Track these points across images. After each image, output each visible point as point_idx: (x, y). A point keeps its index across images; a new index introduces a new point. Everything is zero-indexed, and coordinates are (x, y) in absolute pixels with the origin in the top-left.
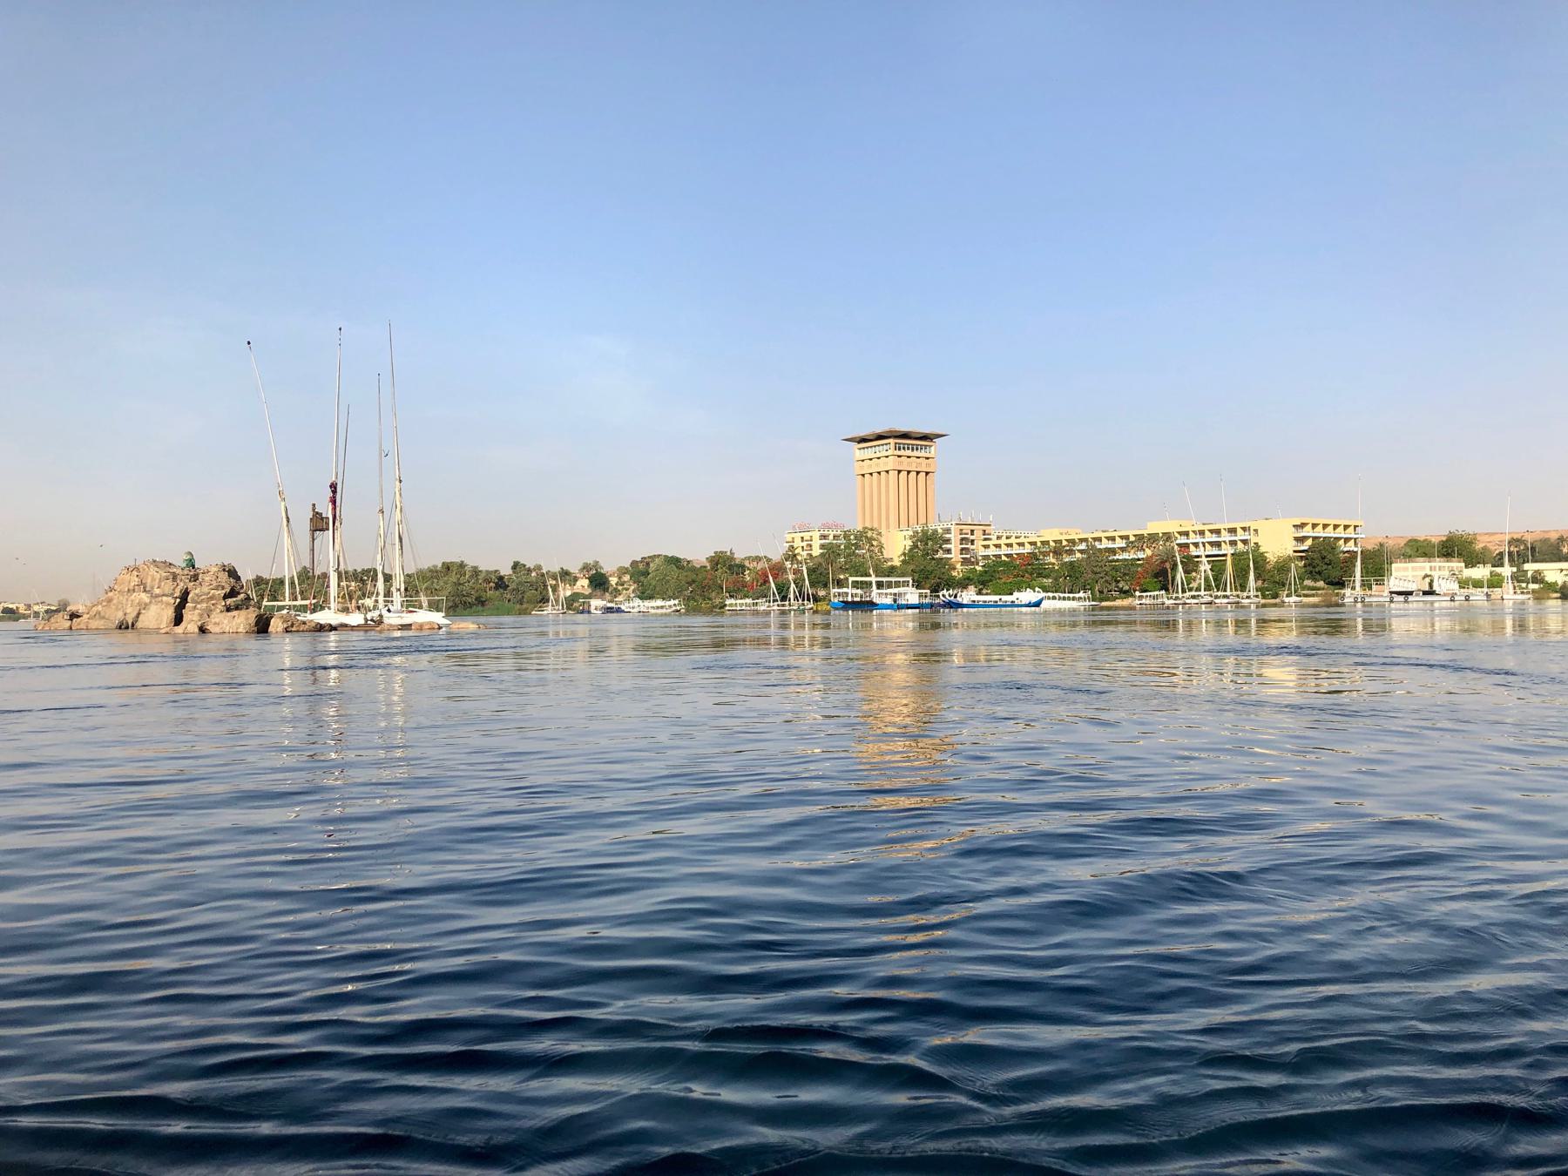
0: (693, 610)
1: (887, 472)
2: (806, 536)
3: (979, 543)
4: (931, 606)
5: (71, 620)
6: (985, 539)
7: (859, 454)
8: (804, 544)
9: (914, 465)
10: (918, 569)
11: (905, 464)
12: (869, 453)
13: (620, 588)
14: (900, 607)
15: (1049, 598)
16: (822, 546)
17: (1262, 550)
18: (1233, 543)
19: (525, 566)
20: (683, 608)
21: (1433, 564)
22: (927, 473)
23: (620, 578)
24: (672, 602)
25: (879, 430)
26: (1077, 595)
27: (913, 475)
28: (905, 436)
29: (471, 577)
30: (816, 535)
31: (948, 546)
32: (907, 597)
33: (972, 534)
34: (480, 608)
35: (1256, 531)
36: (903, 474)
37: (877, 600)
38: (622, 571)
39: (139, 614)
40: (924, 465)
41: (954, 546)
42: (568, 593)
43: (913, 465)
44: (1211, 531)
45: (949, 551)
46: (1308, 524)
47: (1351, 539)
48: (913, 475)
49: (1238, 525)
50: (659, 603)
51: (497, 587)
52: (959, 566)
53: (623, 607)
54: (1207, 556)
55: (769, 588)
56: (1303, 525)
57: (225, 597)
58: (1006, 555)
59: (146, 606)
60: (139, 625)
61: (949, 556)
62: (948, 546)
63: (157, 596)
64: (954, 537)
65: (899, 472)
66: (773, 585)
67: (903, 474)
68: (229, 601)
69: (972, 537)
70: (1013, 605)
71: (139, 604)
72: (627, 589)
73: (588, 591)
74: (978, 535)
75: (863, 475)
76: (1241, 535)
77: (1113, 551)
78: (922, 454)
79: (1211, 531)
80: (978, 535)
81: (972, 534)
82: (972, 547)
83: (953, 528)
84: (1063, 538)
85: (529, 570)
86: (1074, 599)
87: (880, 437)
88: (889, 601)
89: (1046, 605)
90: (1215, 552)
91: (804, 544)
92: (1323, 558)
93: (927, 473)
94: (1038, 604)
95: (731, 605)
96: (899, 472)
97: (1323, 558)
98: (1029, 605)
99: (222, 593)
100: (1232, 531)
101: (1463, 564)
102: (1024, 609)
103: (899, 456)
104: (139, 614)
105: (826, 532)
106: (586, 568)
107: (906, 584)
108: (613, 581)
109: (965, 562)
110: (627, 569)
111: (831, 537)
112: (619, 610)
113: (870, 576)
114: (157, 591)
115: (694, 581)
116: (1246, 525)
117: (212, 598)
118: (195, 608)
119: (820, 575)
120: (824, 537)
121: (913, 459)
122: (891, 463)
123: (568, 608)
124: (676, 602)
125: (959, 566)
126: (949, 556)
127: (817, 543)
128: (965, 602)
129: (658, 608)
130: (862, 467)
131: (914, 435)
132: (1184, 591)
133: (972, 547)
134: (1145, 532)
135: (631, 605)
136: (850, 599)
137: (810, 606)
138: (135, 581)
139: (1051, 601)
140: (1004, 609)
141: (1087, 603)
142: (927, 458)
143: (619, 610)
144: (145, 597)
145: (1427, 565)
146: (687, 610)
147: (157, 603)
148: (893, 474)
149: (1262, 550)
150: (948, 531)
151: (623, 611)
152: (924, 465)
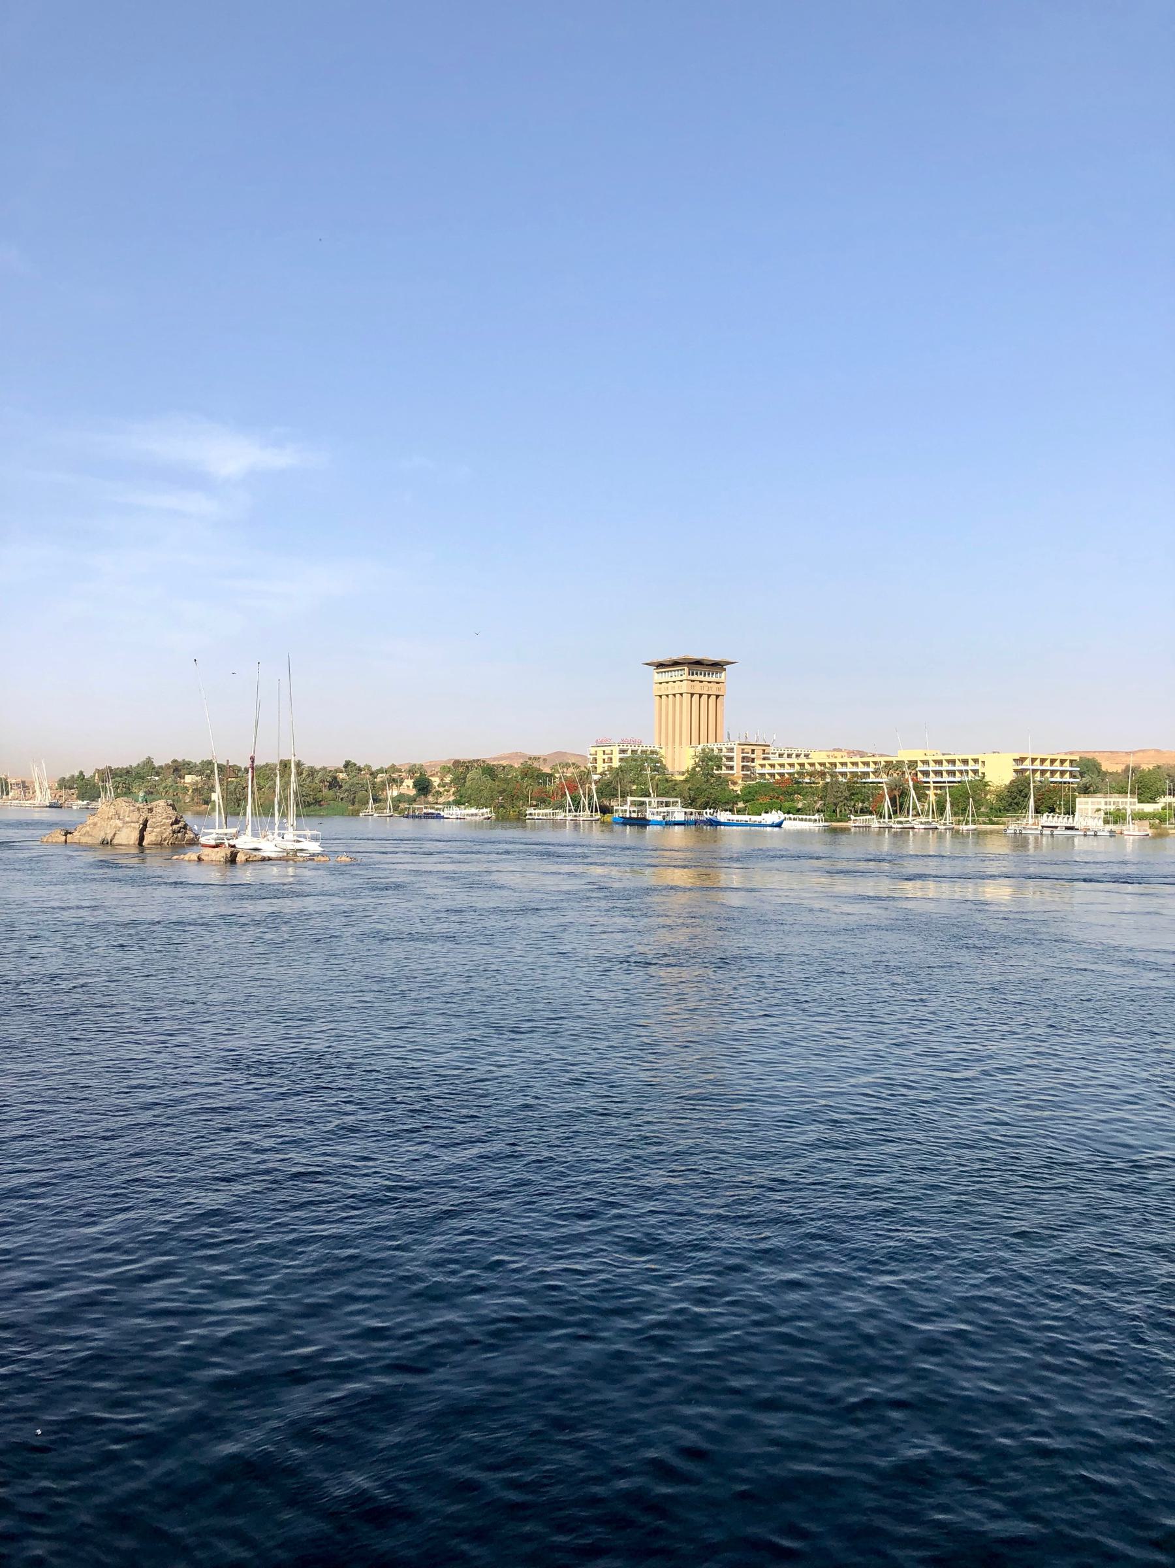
0: (502, 819)
1: (681, 694)
2: (608, 750)
3: (758, 762)
4: (695, 823)
5: (66, 835)
6: (764, 759)
7: (658, 677)
8: (606, 757)
9: (706, 688)
10: (694, 788)
11: (698, 687)
12: (666, 677)
13: (441, 789)
14: (669, 824)
15: (790, 819)
16: (621, 760)
17: (987, 779)
18: (938, 773)
19: (355, 765)
20: (493, 816)
21: (1108, 800)
22: (717, 696)
23: (442, 780)
24: (485, 810)
25: (675, 657)
26: (813, 817)
27: (704, 698)
28: (698, 663)
29: (308, 775)
30: (616, 749)
31: (731, 763)
32: (676, 814)
33: (753, 753)
34: (317, 807)
35: (983, 762)
36: (696, 697)
37: (649, 817)
38: (445, 770)
39: (115, 834)
40: (714, 689)
41: (737, 763)
42: (395, 793)
43: (705, 689)
44: (949, 761)
45: (731, 768)
46: (1026, 758)
47: (1067, 771)
48: (704, 698)
49: (969, 757)
50: (473, 811)
51: (330, 787)
52: (740, 782)
53: (442, 814)
54: (934, 782)
55: (566, 799)
56: (1022, 760)
57: (172, 824)
58: (788, 773)
59: (119, 829)
60: (115, 842)
61: (731, 772)
62: (731, 763)
63: (128, 822)
64: (737, 755)
65: (692, 695)
66: (569, 798)
67: (696, 697)
68: (175, 827)
69: (753, 756)
70: (760, 825)
71: (115, 827)
72: (448, 791)
73: (413, 792)
74: (758, 753)
75: (660, 696)
76: (971, 766)
77: (866, 774)
78: (713, 678)
79: (949, 761)
80: (758, 753)
81: (753, 753)
82: (753, 764)
83: (735, 747)
84: (827, 761)
85: (360, 770)
86: (810, 820)
87: (676, 663)
88: (659, 818)
89: (786, 825)
90: (939, 779)
91: (606, 757)
92: (1021, 791)
93: (717, 696)
94: (779, 825)
95: (531, 814)
96: (692, 695)
97: (1021, 791)
98: (772, 826)
99: (170, 821)
100: (965, 762)
101: (1136, 800)
102: (769, 829)
103: (693, 681)
104: (115, 834)
105: (625, 748)
106: (411, 771)
107: (675, 804)
108: (436, 781)
109: (745, 777)
110: (449, 768)
111: (629, 752)
112: (439, 817)
113: (649, 796)
114: (127, 819)
115: (504, 791)
116: (975, 757)
117: (163, 825)
118: (153, 831)
119: (609, 789)
120: (623, 751)
121: (705, 682)
122: (684, 687)
123: (394, 810)
124: (488, 810)
125: (740, 782)
126: (731, 772)
127: (616, 757)
128: (722, 820)
129: (472, 815)
130: (660, 689)
131: (705, 662)
132: (890, 817)
133: (753, 764)
134: (894, 759)
135: (451, 812)
136: (628, 816)
137: (597, 817)
138: (112, 811)
139: (792, 822)
140: (753, 828)
141: (822, 824)
142: (718, 683)
143: (439, 817)
144: (119, 823)
145: (1103, 800)
146: (497, 819)
147: (127, 827)
148: (686, 697)
149: (987, 779)
150: (731, 750)
151: (443, 817)
152: (714, 689)
